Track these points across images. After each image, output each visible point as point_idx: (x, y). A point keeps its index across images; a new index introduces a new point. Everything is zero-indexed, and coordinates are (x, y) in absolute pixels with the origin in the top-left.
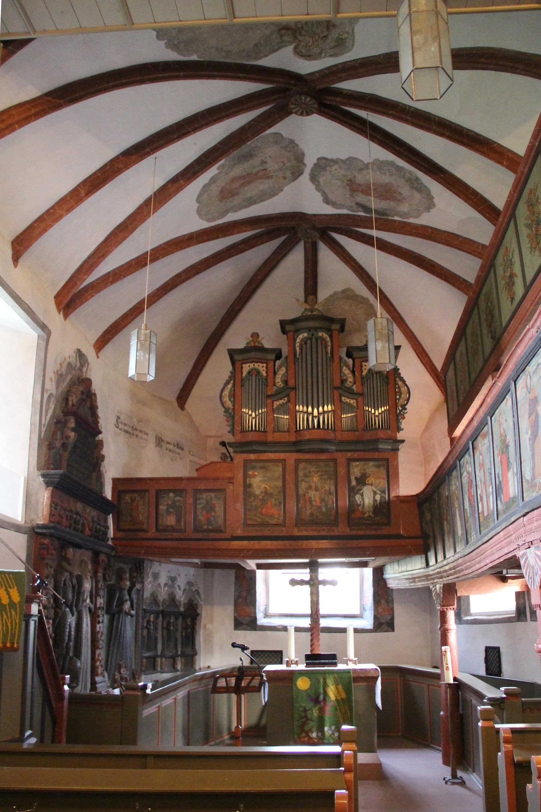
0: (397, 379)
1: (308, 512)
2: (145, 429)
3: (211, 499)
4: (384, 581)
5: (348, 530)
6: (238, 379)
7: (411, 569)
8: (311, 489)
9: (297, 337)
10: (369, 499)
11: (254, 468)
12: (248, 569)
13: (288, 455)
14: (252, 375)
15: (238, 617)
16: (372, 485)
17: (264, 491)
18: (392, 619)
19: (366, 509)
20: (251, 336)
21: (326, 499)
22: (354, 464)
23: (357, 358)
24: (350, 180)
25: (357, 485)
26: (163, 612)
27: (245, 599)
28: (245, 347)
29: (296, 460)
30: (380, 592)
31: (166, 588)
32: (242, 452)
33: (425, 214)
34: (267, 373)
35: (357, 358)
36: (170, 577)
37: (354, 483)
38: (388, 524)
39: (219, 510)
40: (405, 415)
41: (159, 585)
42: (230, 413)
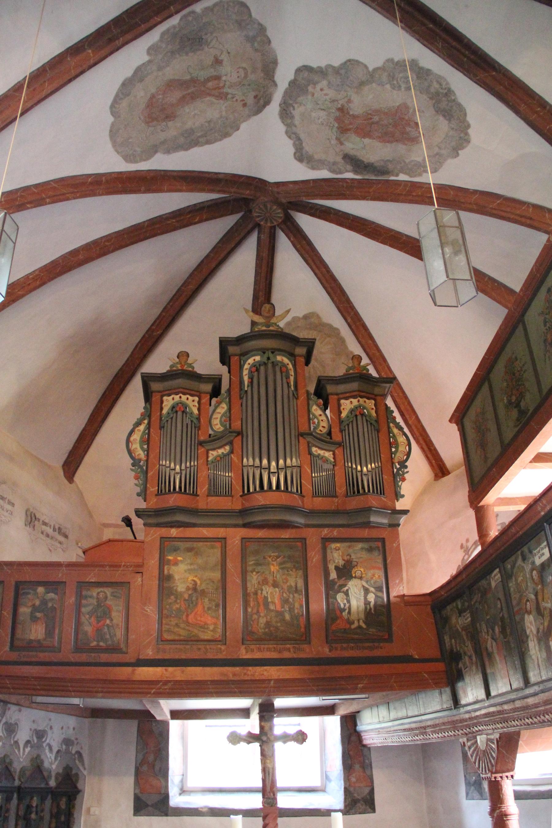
0: (391, 425)
1: (263, 621)
2: (11, 497)
3: (106, 598)
4: (358, 735)
5: (327, 650)
6: (155, 417)
7: (416, 713)
8: (267, 583)
9: (245, 362)
10: (358, 600)
11: (176, 549)
12: (158, 718)
13: (230, 530)
14: (177, 412)
15: (140, 795)
16: (361, 578)
17: (191, 586)
18: (372, 792)
19: (353, 617)
20: (178, 357)
21: (291, 600)
22: (333, 546)
23: (332, 394)
24: (341, 110)
25: (339, 577)
26: (19, 789)
27: (152, 766)
28: (168, 371)
29: (242, 539)
30: (351, 753)
31: (28, 750)
32: (158, 525)
33: (450, 161)
34: (199, 409)
35: (332, 394)
36: (35, 730)
37: (333, 575)
38: (389, 639)
39: (117, 616)
40: (406, 475)
41: (16, 742)
42: (141, 467)
